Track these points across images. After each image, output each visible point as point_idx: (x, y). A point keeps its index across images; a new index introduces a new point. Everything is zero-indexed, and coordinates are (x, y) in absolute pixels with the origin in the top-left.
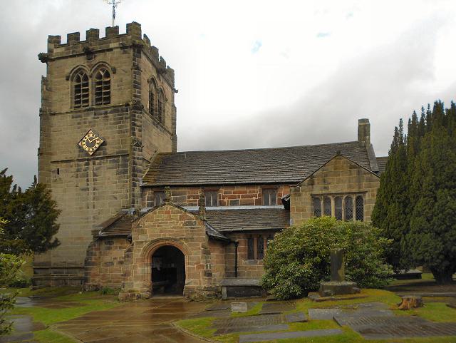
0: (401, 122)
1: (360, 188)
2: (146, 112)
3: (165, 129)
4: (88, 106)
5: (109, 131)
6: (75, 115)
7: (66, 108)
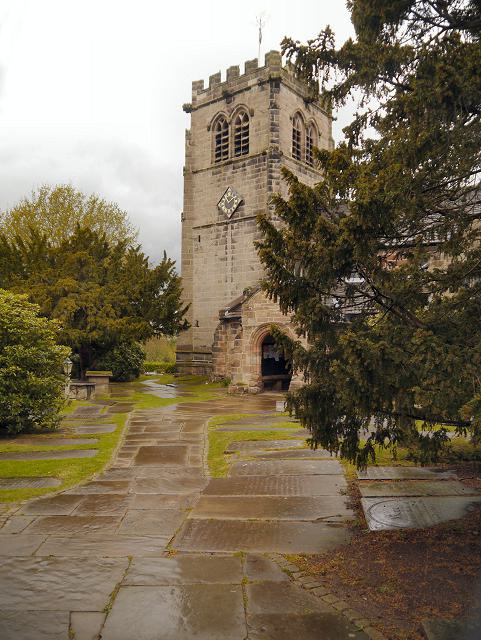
2: (287, 158)
5: (247, 187)
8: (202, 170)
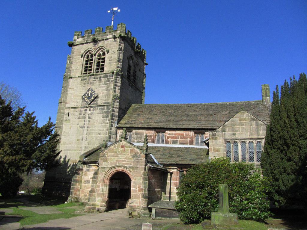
0: (277, 88)
1: (258, 135)
3: (137, 89)
4: (91, 73)
6: (83, 78)
7: (79, 74)
8: (75, 77)
